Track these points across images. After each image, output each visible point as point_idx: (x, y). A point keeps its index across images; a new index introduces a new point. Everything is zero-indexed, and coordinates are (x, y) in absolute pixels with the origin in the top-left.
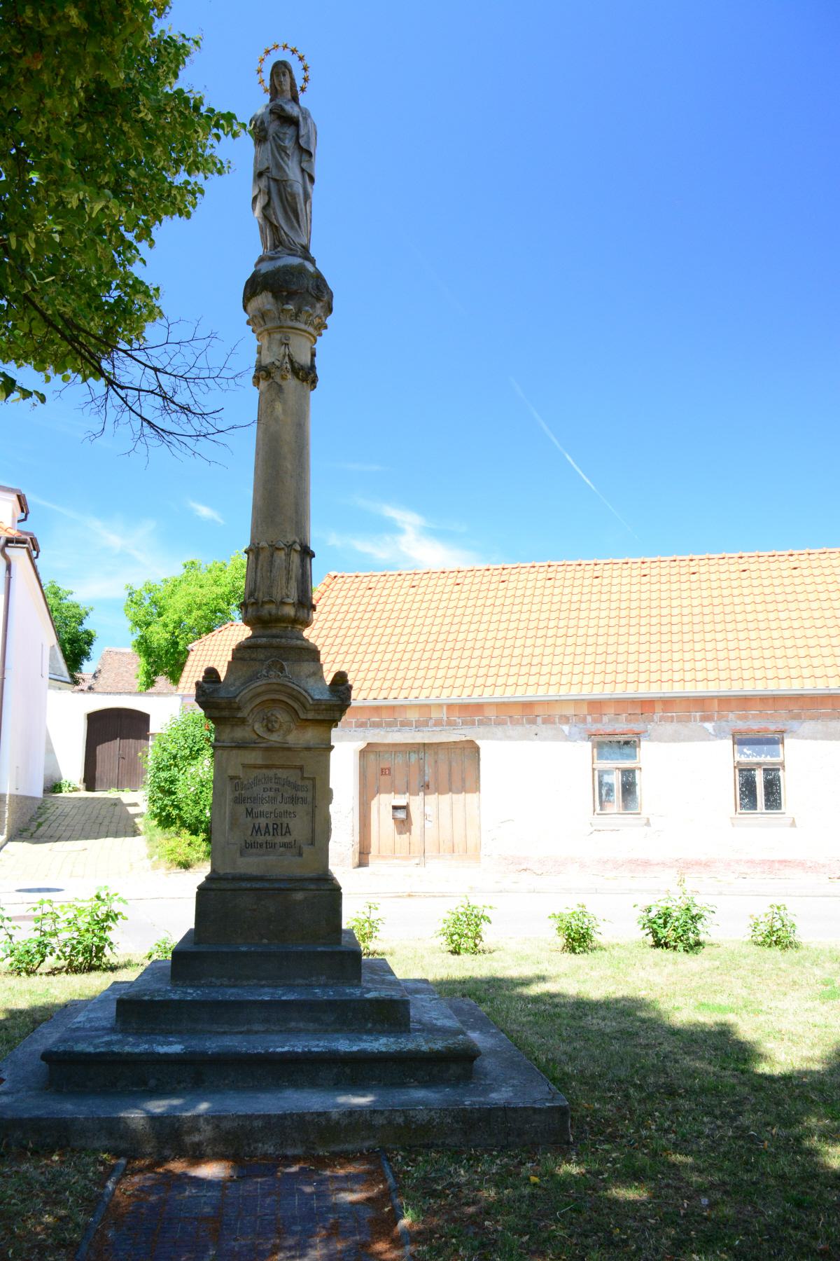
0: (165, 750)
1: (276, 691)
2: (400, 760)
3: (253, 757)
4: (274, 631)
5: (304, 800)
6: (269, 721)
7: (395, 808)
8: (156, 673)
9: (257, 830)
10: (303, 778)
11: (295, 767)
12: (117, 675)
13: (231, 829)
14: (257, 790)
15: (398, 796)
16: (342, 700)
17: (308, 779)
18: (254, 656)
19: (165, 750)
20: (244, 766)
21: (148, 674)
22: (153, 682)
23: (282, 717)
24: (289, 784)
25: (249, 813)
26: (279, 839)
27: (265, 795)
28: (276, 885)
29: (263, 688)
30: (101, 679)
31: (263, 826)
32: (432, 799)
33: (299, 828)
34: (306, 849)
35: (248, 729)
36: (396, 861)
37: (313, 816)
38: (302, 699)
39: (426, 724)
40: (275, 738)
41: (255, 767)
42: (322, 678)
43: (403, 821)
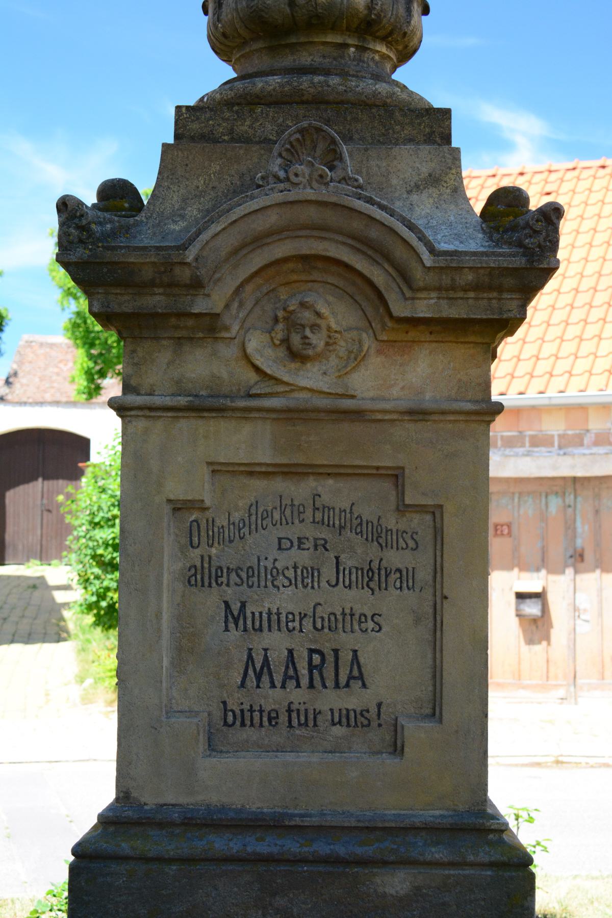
0: (103, 490)
1: (320, 229)
2: (529, 508)
3: (243, 442)
4: (305, 59)
5: (406, 578)
6: (292, 323)
7: (521, 596)
8: (102, 374)
9: (258, 670)
10: (403, 508)
11: (377, 473)
12: (42, 379)
13: (178, 664)
14: (260, 546)
15: (525, 575)
16: (528, 253)
17: (420, 509)
18: (243, 127)
19: (103, 490)
20: (217, 469)
21: (90, 375)
22: (98, 388)
23: (335, 313)
24: (359, 526)
25: (234, 616)
26: (331, 700)
27: (284, 560)
28: (322, 848)
29: (272, 219)
30: (17, 386)
31: (278, 657)
32: (590, 580)
33: (390, 665)
34: (416, 733)
35: (229, 352)
36: (523, 693)
37: (437, 627)
38: (399, 252)
39: (578, 441)
40: (312, 378)
41: (251, 471)
42: (458, 190)
43: (534, 621)
